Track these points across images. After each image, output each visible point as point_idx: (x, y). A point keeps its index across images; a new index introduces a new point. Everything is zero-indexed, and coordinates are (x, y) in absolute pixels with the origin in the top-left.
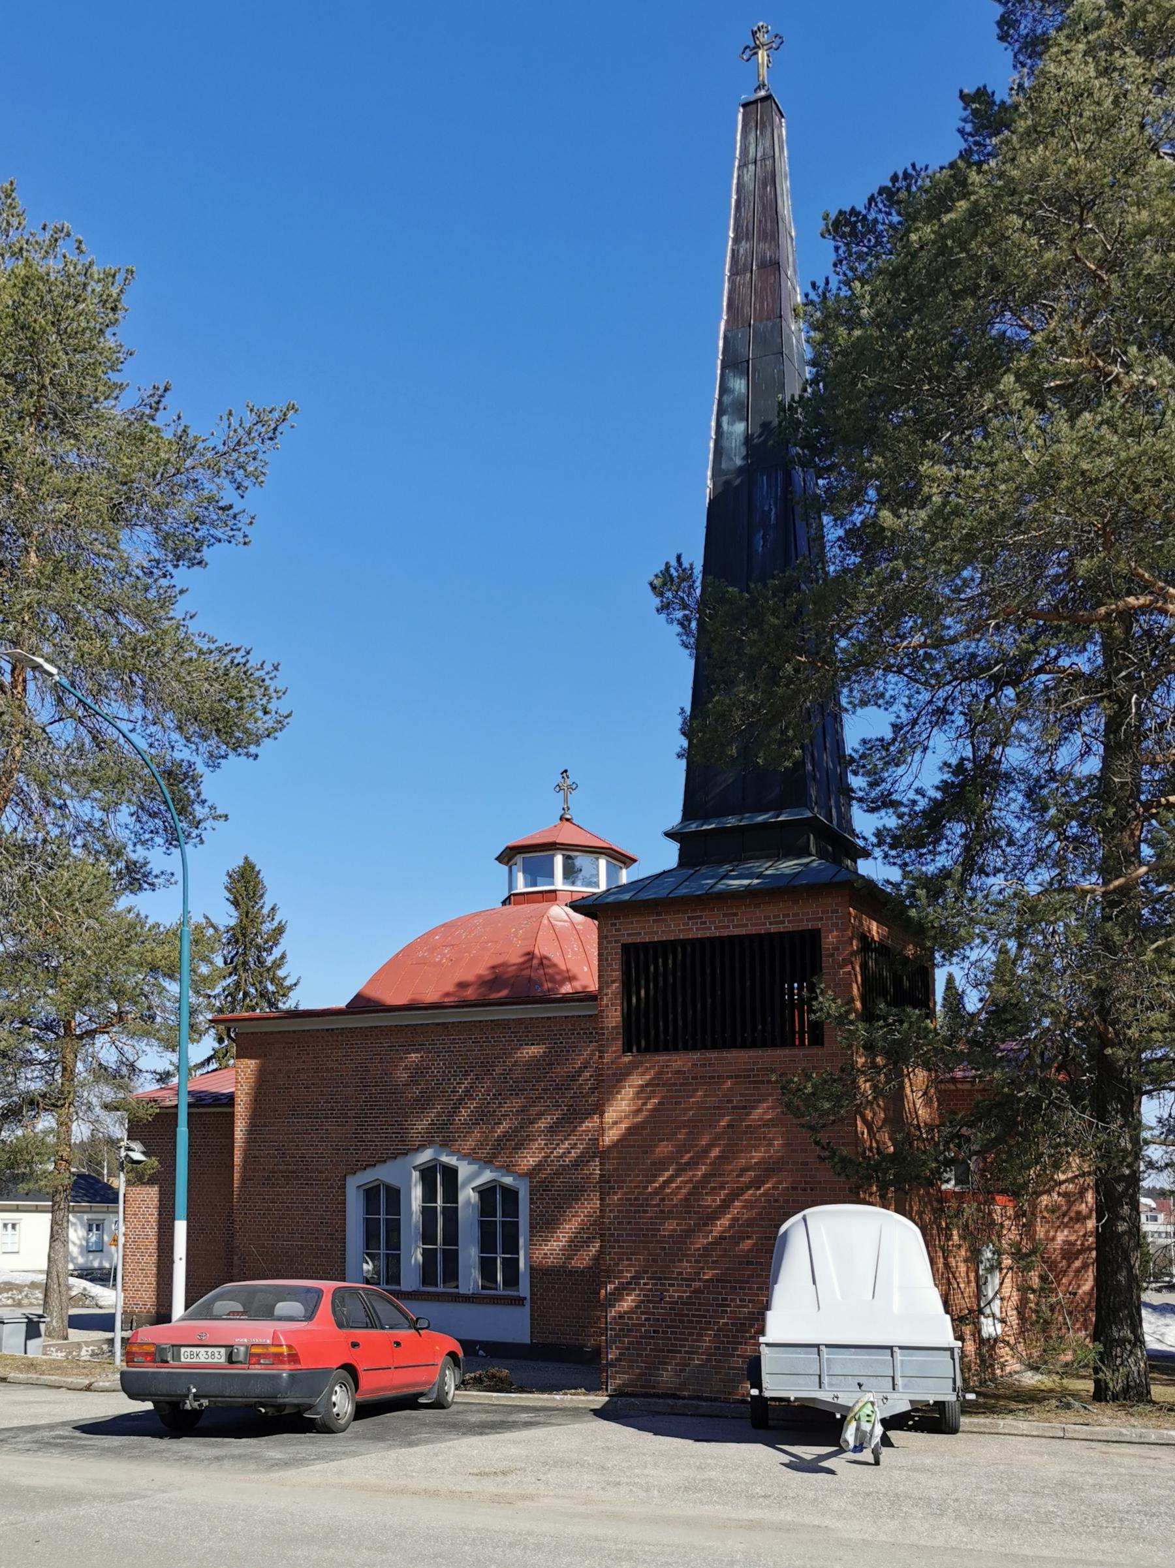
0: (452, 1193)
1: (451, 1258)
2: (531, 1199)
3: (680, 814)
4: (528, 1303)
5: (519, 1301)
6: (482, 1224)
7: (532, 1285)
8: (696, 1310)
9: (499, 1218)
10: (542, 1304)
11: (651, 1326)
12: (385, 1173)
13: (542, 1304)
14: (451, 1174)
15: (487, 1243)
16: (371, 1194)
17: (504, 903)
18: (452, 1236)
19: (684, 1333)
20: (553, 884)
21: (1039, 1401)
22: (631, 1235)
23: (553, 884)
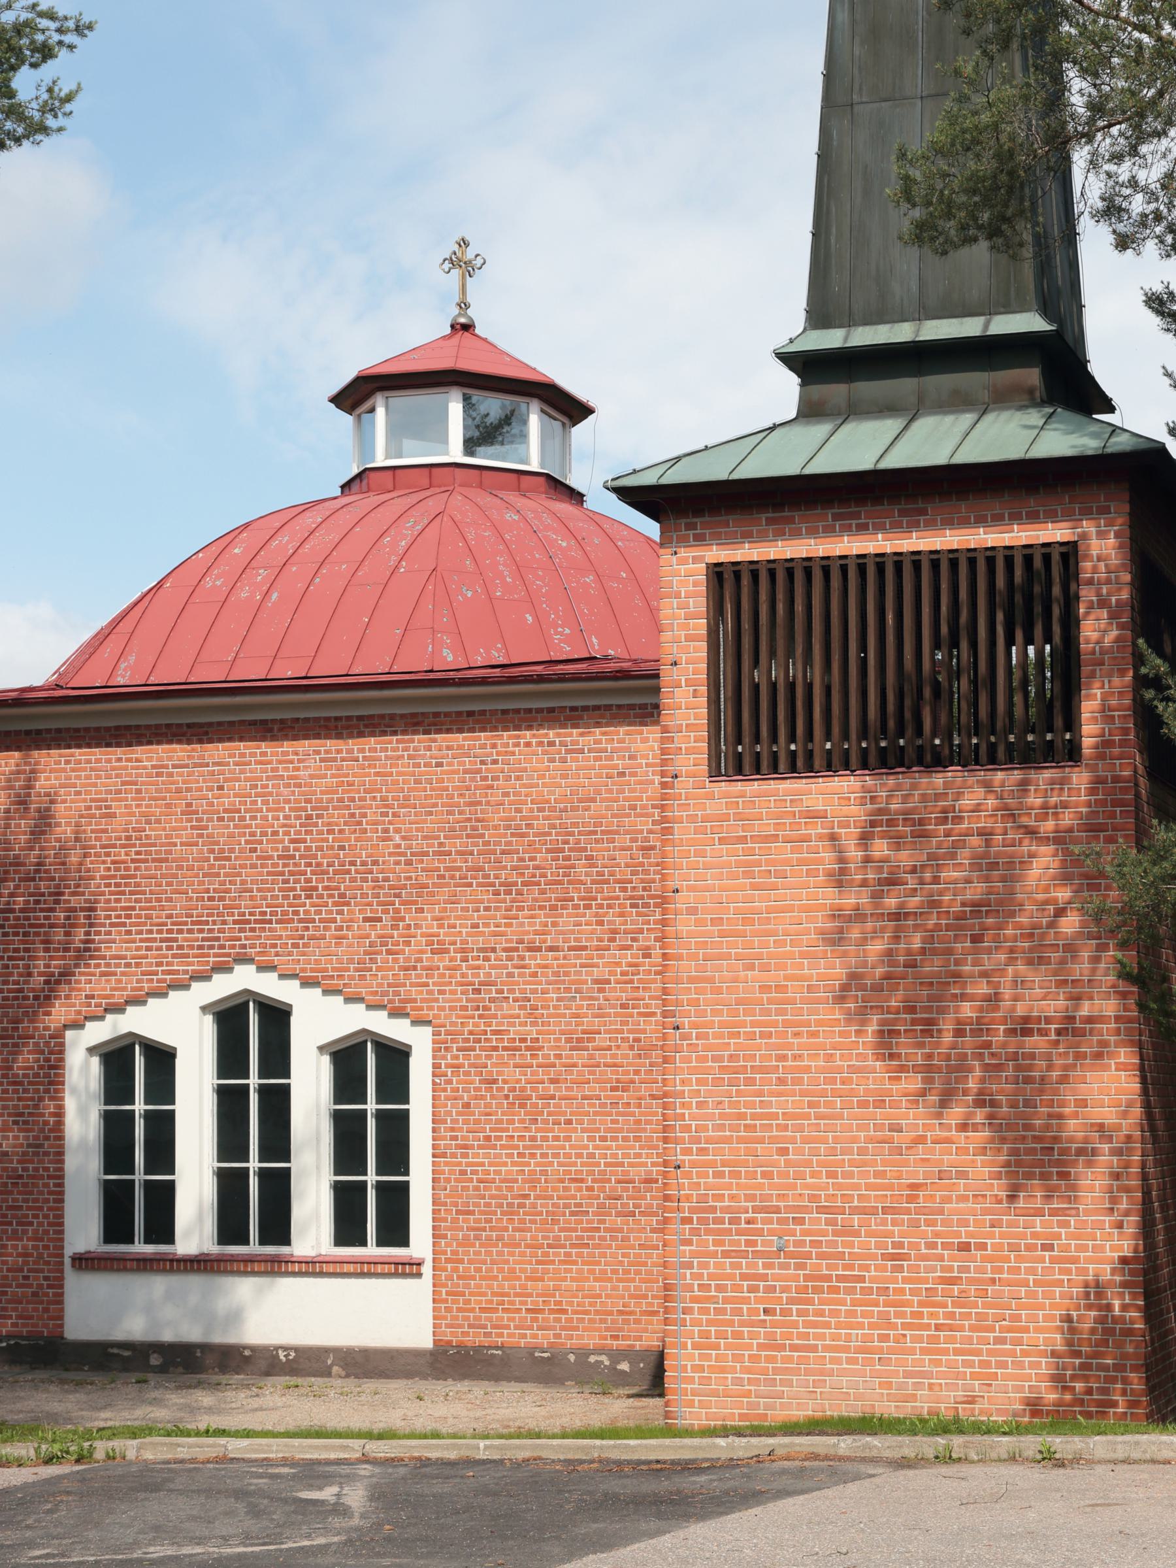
0: (277, 1057)
1: (278, 1189)
2: (436, 1066)
3: (802, 316)
4: (427, 1269)
5: (411, 1269)
6: (338, 1118)
7: (437, 1235)
8: (845, 1267)
9: (371, 1106)
10: (455, 1270)
11: (758, 1300)
12: (152, 1021)
13: (455, 1270)
14: (277, 1017)
15: (348, 1151)
16: (116, 1058)
17: (346, 487)
18: (278, 1140)
19: (821, 1313)
20: (447, 453)
21: (155, 1488)
22: (721, 1128)
23: (447, 453)
